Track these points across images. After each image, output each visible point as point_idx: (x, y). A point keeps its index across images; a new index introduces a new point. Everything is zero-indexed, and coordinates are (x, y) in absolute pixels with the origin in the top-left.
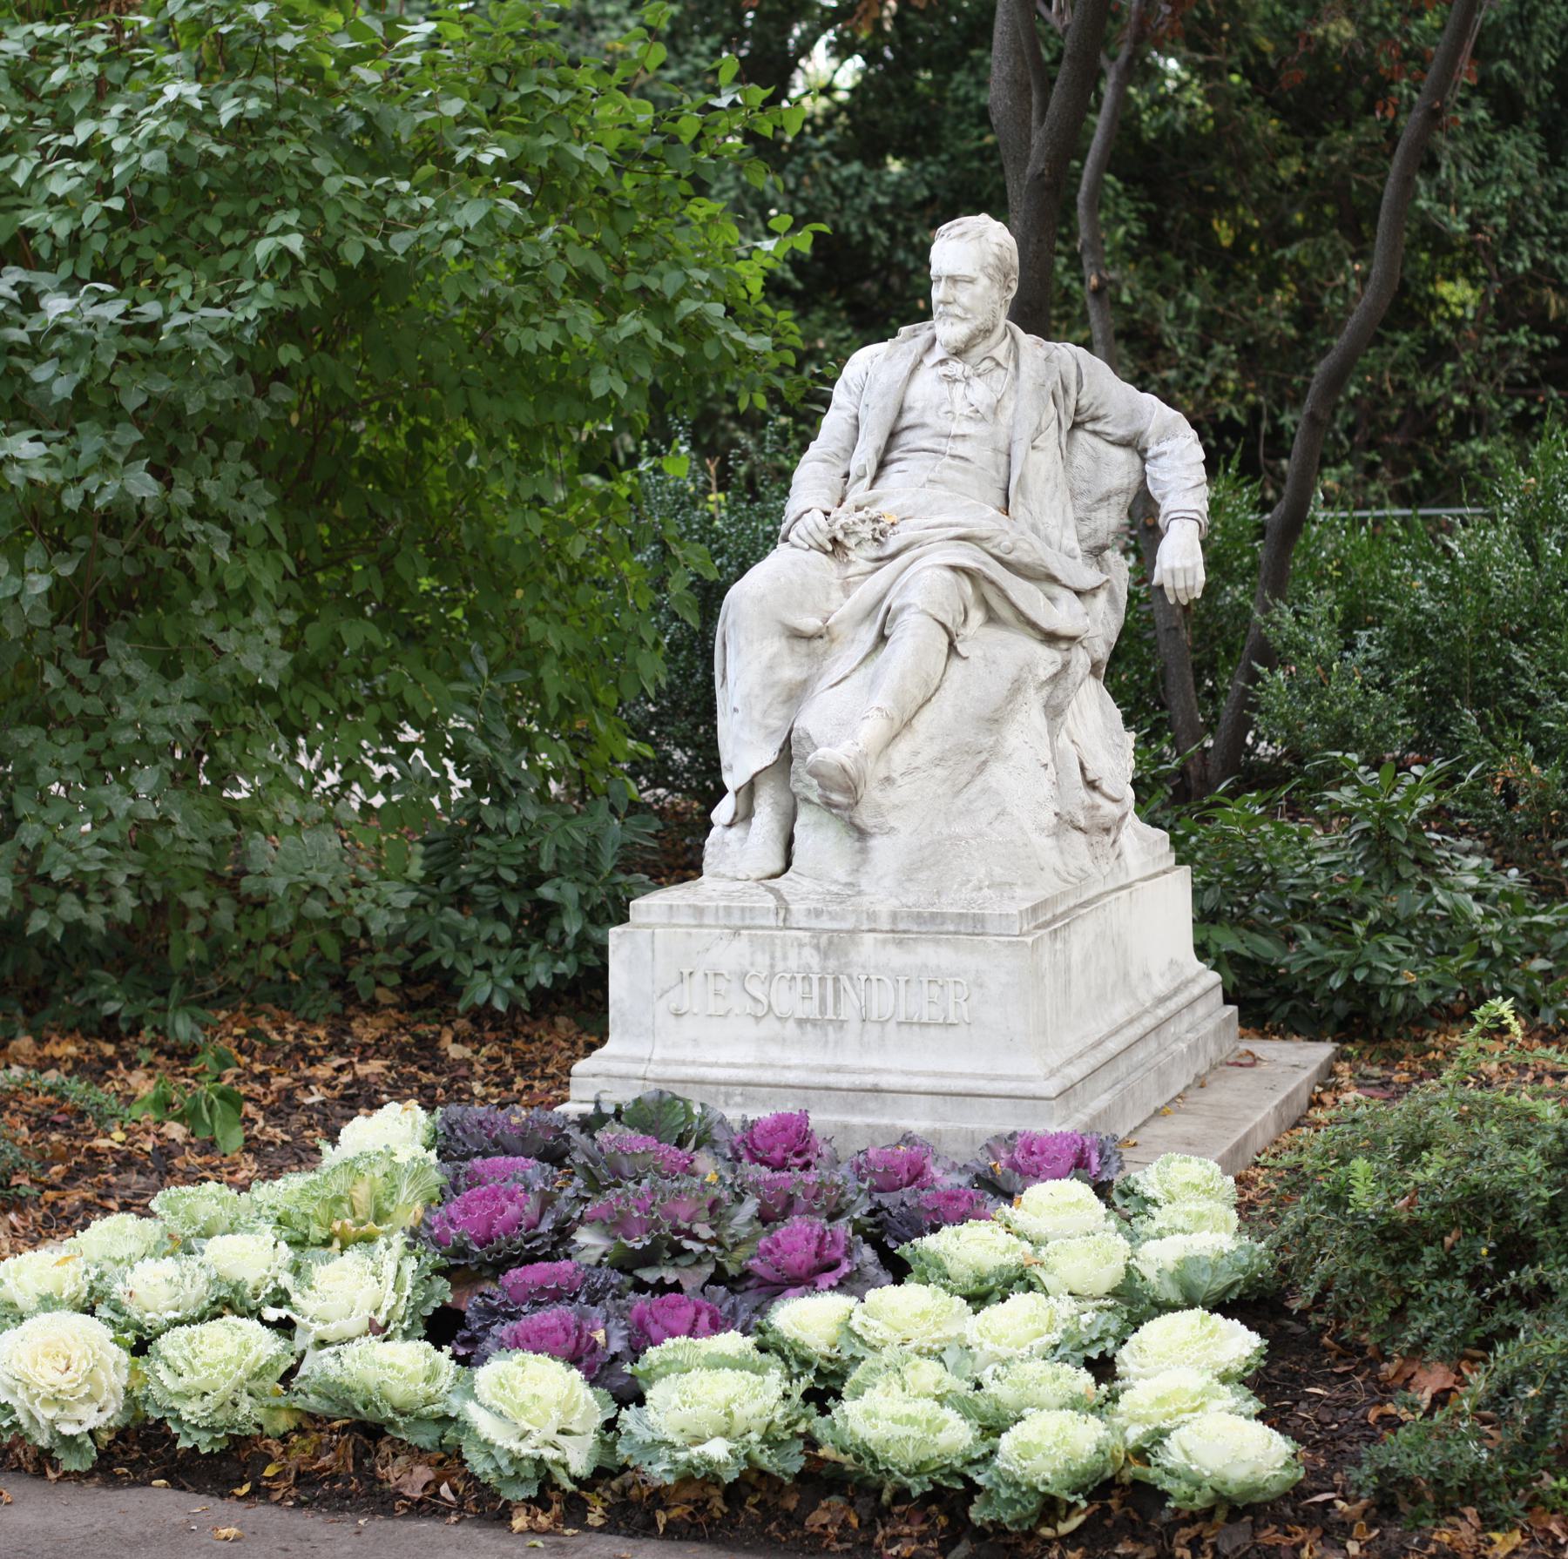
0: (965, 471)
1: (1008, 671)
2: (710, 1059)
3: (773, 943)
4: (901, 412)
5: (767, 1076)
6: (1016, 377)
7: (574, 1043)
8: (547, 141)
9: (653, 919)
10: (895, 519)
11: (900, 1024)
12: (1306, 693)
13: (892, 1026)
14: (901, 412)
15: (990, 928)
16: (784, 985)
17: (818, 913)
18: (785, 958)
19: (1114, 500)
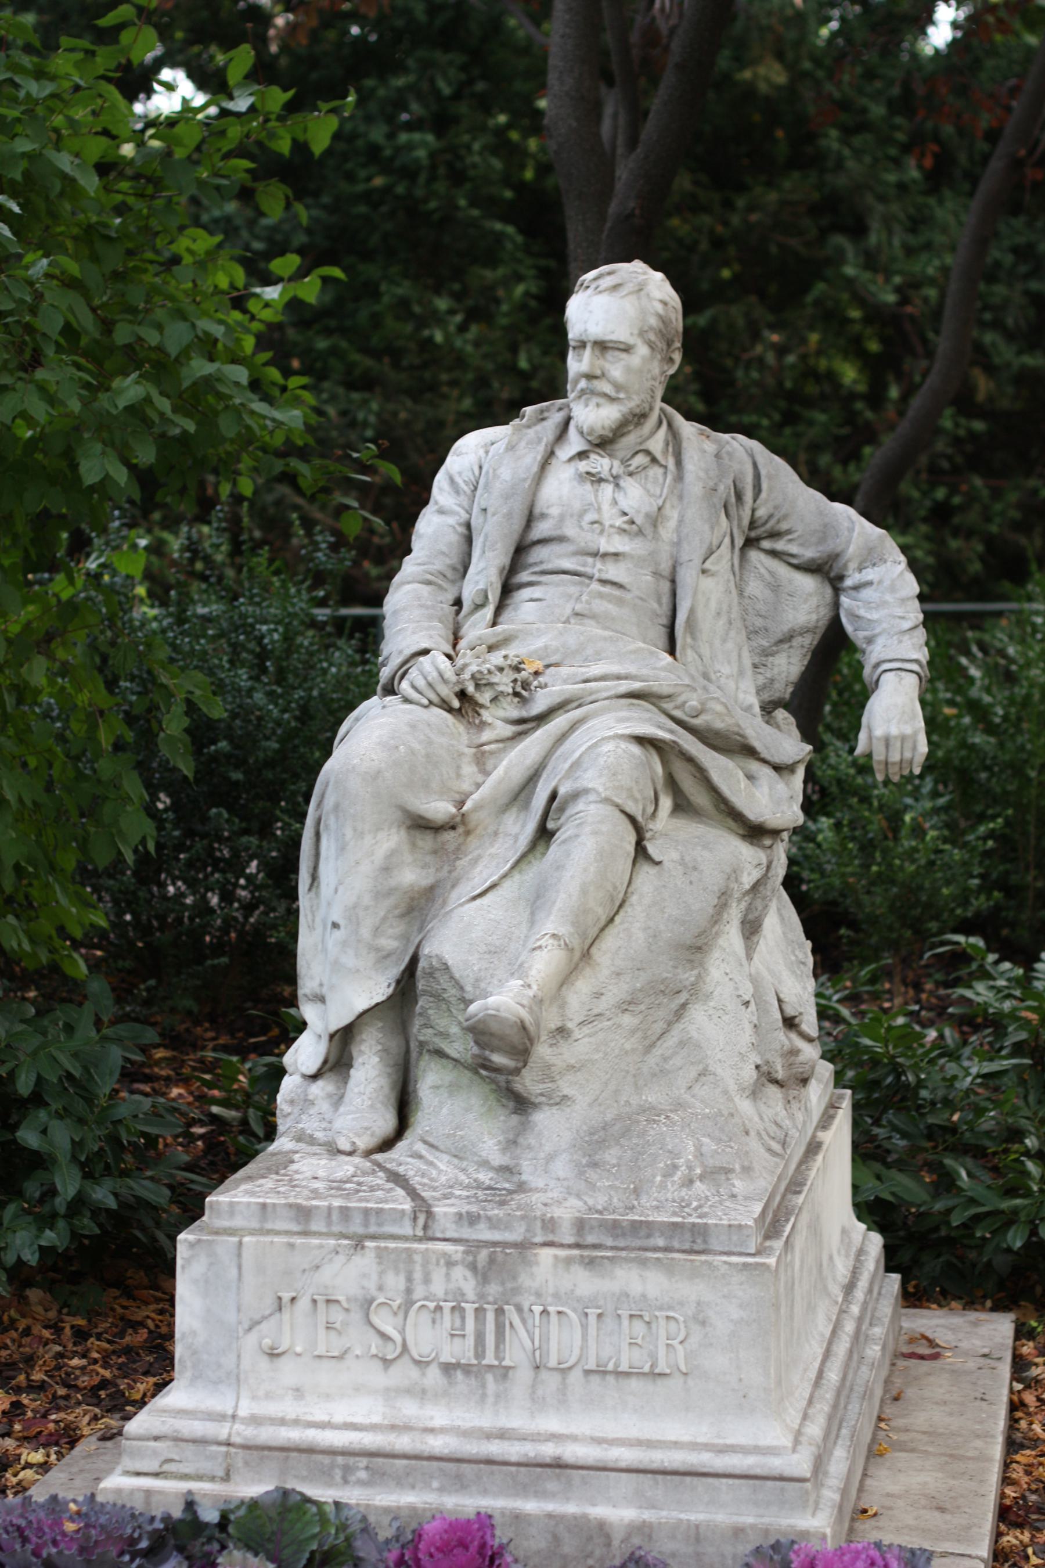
0: (620, 602)
1: (713, 879)
2: (320, 1416)
3: (410, 1260)
4: (530, 519)
5: (404, 1443)
6: (679, 477)
7: (58, 1330)
8: (23, 146)
9: (238, 1222)
10: (539, 665)
11: (588, 1372)
12: (867, 847)
13: (576, 1375)
14: (530, 519)
15: (715, 1244)
16: (425, 1317)
17: (472, 1219)
18: (427, 1280)
19: (797, 641)
